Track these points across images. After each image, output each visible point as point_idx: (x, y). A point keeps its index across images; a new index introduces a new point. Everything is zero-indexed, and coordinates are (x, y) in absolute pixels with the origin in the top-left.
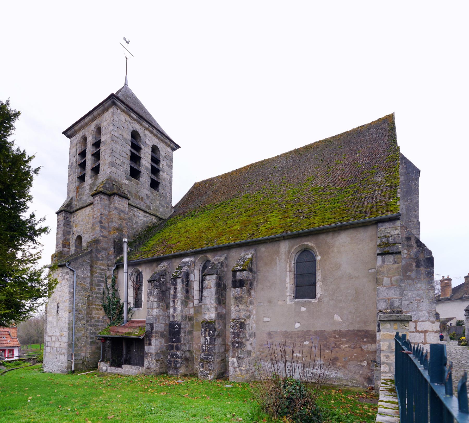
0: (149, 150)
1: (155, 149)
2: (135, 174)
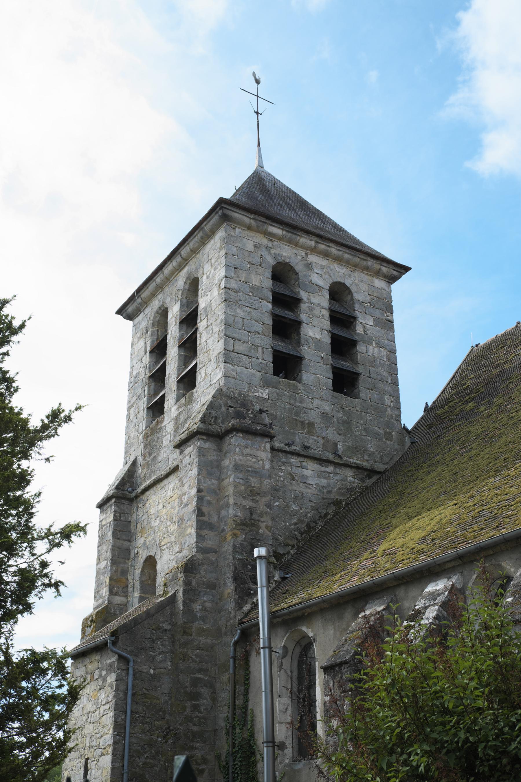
1: (338, 292)
2: (286, 365)
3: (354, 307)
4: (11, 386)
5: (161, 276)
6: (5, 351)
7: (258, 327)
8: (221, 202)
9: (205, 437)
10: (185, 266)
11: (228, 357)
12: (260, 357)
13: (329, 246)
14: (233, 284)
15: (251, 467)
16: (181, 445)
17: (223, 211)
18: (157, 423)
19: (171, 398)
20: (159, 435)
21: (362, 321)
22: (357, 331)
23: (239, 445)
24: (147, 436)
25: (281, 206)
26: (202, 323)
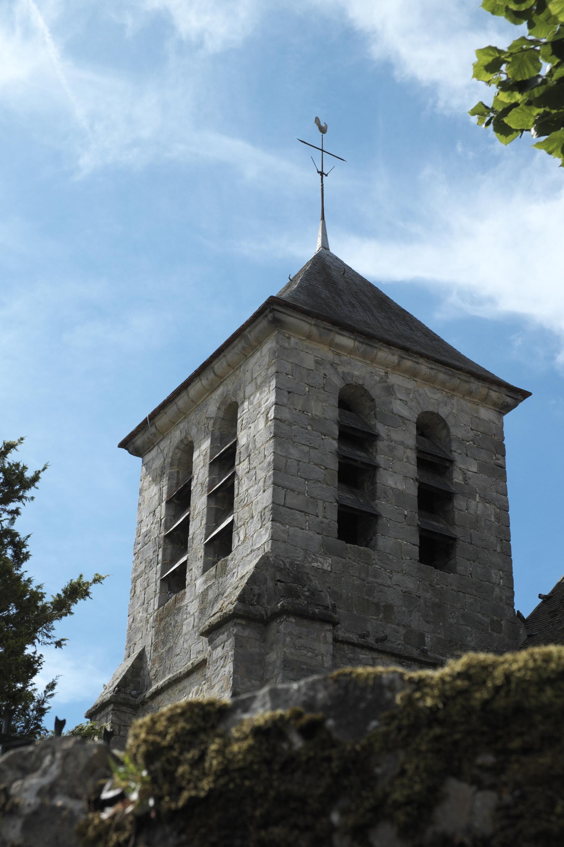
0: (408, 437)
1: (429, 427)
2: (355, 526)
3: (451, 446)
4: (20, 551)
5: (186, 397)
6: (14, 509)
7: (319, 473)
8: (272, 304)
9: (243, 622)
10: (219, 386)
11: (279, 513)
12: (321, 514)
13: (418, 363)
14: (286, 415)
15: (306, 664)
16: (211, 632)
17: (272, 312)
18: (175, 601)
19: (196, 566)
20: (178, 618)
21: (462, 466)
22: (455, 480)
23: (290, 634)
24: (160, 619)
25: (353, 306)
26: (241, 465)
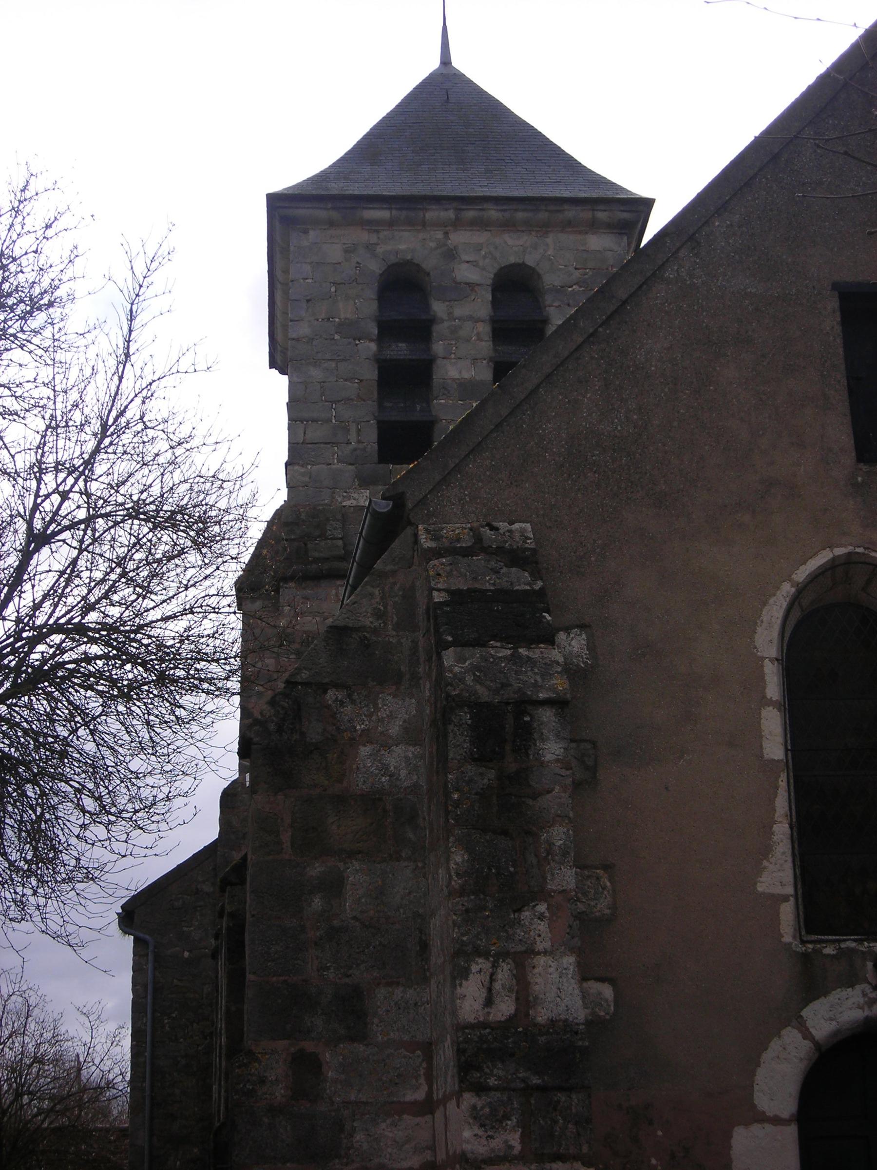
0: (480, 306)
